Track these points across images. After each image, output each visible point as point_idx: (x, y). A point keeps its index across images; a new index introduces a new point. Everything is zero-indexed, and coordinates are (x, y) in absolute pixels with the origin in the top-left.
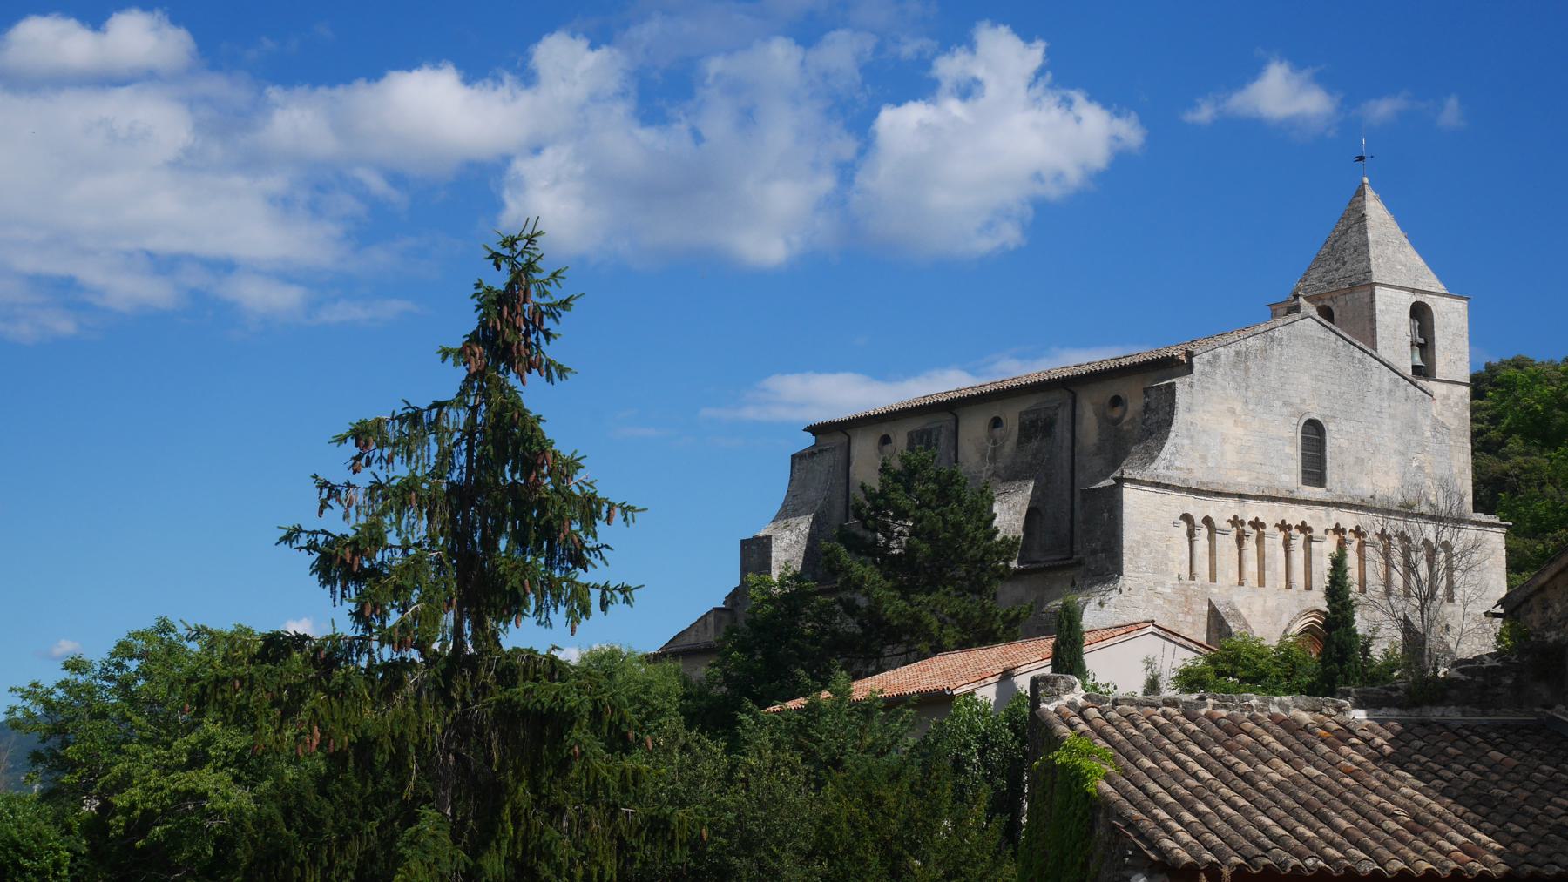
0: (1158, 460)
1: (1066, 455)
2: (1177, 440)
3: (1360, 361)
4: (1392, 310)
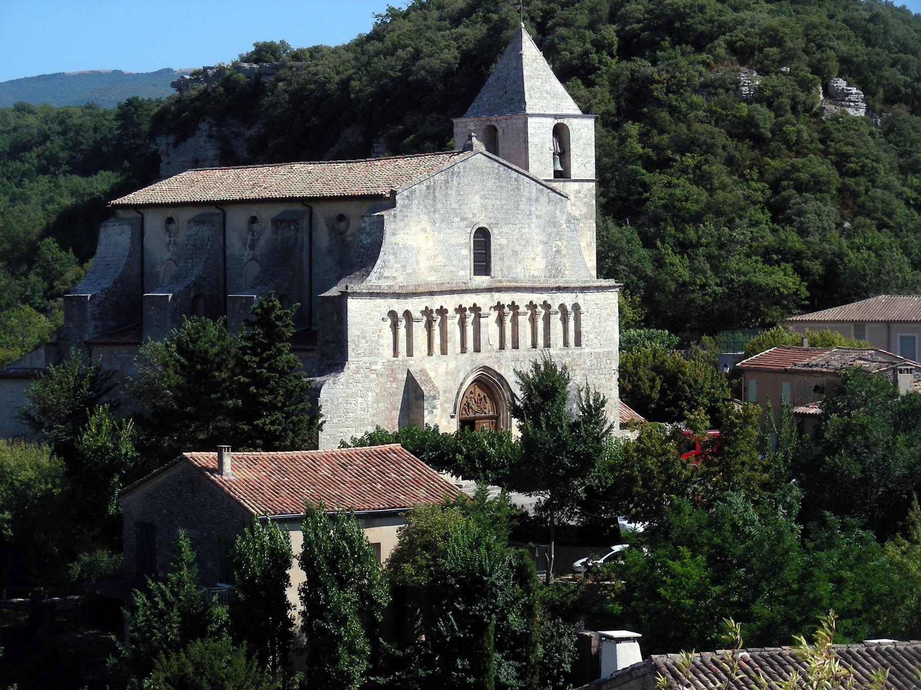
0: (372, 274)
1: (305, 254)
2: (386, 257)
3: (516, 180)
4: (539, 135)
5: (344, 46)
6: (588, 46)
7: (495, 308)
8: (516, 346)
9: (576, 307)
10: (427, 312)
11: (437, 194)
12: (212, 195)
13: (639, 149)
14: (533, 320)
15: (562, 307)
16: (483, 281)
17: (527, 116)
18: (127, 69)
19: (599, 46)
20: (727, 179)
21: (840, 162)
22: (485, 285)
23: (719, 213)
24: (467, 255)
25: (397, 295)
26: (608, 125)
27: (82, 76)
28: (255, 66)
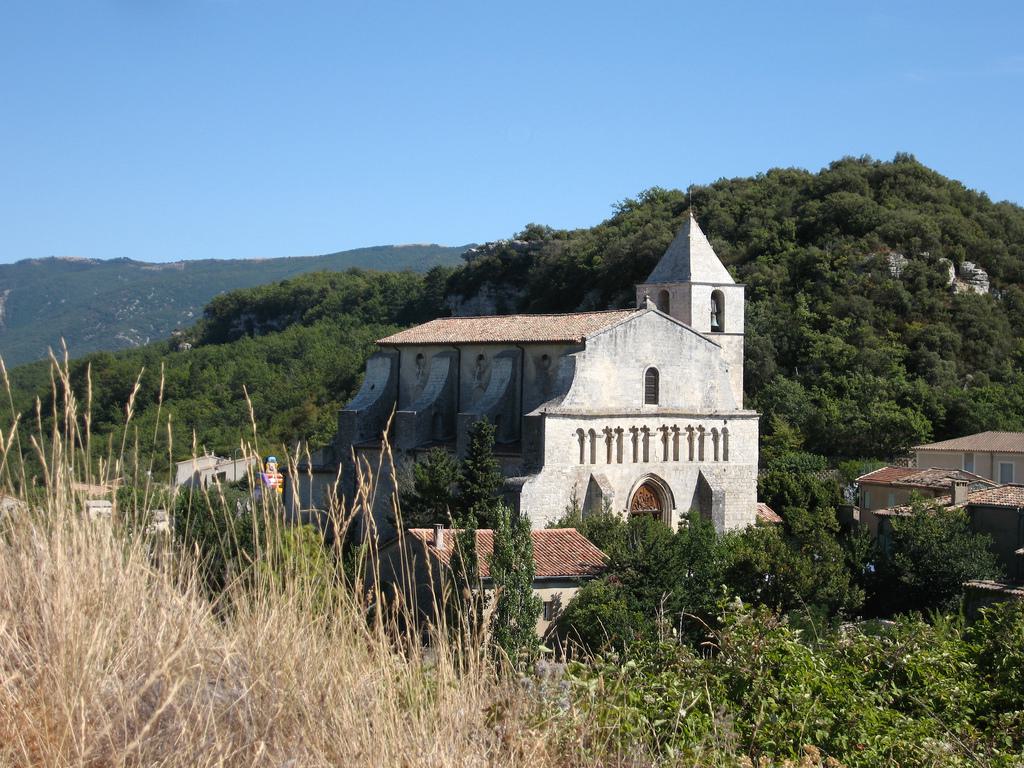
4: (701, 300)
5: (592, 229)
6: (774, 234)
7: (661, 429)
8: (676, 458)
9: (725, 431)
10: (607, 431)
11: (618, 341)
12: (451, 338)
13: (807, 314)
14: (691, 439)
15: (714, 431)
16: (652, 408)
17: (691, 284)
18: (442, 244)
19: (783, 234)
20: (873, 338)
21: (964, 327)
22: (654, 412)
23: (865, 364)
24: (640, 389)
25: (584, 417)
26: (751, 296)
27: (406, 249)
28: (525, 243)
